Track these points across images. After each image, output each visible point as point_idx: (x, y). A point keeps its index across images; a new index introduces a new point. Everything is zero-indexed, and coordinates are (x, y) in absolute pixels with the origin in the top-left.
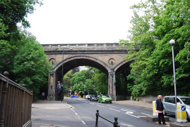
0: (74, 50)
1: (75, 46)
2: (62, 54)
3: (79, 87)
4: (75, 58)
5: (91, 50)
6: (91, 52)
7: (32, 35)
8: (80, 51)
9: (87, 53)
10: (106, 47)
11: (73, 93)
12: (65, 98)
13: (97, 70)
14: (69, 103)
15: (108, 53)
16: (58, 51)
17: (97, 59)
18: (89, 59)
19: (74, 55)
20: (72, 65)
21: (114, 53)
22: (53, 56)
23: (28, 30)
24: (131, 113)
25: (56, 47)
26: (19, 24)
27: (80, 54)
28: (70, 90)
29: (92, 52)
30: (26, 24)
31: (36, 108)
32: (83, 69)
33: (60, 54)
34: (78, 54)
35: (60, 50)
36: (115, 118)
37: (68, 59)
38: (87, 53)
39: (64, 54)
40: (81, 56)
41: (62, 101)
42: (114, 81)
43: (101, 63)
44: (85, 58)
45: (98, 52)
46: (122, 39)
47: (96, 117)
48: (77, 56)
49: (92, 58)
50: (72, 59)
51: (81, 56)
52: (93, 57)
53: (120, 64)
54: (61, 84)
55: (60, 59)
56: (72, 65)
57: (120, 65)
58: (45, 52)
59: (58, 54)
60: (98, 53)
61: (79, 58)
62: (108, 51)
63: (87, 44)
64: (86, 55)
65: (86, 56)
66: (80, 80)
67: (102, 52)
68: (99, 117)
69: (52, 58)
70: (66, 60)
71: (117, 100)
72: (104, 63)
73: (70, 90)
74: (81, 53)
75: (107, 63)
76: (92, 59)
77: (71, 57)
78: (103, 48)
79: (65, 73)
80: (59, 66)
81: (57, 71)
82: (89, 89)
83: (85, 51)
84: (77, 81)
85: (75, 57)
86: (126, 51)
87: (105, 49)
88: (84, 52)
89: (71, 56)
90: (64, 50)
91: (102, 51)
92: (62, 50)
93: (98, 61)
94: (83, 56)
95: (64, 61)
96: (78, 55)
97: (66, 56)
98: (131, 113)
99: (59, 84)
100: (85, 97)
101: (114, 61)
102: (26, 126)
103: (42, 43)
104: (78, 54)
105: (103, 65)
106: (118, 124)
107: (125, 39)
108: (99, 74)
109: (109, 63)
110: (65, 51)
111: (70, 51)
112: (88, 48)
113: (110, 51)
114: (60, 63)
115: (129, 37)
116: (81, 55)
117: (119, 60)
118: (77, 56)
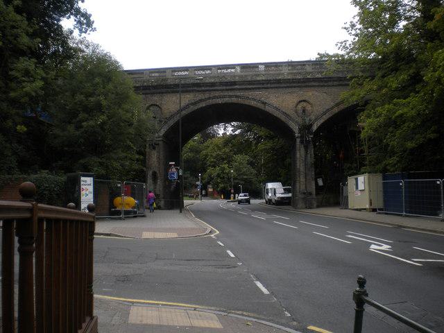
0: (207, 81)
1: (208, 72)
2: (177, 92)
3: (218, 176)
4: (211, 102)
5: (249, 79)
6: (250, 87)
7: (101, 49)
8: (221, 84)
9: (239, 89)
10: (287, 71)
11: (204, 187)
12: (187, 202)
13: (263, 132)
14: (200, 214)
15: (295, 87)
16: (168, 86)
17: (264, 103)
18: (247, 102)
19: (207, 95)
20: (200, 120)
21: (309, 86)
22: (156, 99)
23: (91, 37)
24: (385, 247)
25: (162, 74)
26: (67, 23)
27: (222, 90)
28: (197, 183)
29: (254, 84)
30: (86, 22)
31: (116, 236)
32: (224, 130)
33: (173, 92)
34: (218, 90)
35: (172, 83)
36: (360, 278)
37: (192, 104)
38: (239, 89)
39: (183, 92)
40: (224, 97)
41: (181, 212)
42: (311, 160)
43: (277, 114)
44: (234, 100)
45: (269, 85)
46: (323, 52)
47: (354, 306)
48: (214, 97)
49: (254, 100)
50: (203, 105)
51: (224, 97)
52: (254, 98)
53: (324, 113)
54: (177, 169)
55: (173, 104)
56: (200, 120)
57: (325, 118)
58: (137, 89)
59: (166, 93)
60: (267, 88)
61: (220, 101)
62: (294, 82)
63: (238, 65)
64: (238, 93)
65: (236, 96)
66: (221, 159)
67: (277, 85)
68: (368, 309)
69: (152, 103)
70: (187, 106)
71: (318, 207)
72: (285, 113)
73: (198, 183)
74: (224, 88)
75: (291, 113)
76: (253, 103)
77: (201, 101)
78: (279, 74)
79: (186, 140)
80: (171, 123)
81: (166, 136)
82: (242, 180)
83: (234, 83)
84: (212, 162)
85: (209, 98)
86: (345, 79)
87: (286, 77)
88: (231, 85)
89: (200, 96)
90: (182, 82)
91: (279, 81)
92: (177, 82)
93: (268, 109)
94: (230, 96)
95: (181, 110)
96: (217, 94)
97: (187, 98)
98: (385, 247)
99: (174, 170)
100: (234, 198)
101: (309, 108)
102: (88, 331)
103: (126, 68)
104: (218, 90)
105: (283, 118)
106: (367, 295)
107: (332, 50)
108: (269, 144)
109: (296, 112)
110: (184, 86)
111: (198, 85)
112: (241, 76)
113: (299, 81)
114: (172, 116)
115: (343, 44)
116: (226, 94)
117: (321, 104)
118: (214, 97)
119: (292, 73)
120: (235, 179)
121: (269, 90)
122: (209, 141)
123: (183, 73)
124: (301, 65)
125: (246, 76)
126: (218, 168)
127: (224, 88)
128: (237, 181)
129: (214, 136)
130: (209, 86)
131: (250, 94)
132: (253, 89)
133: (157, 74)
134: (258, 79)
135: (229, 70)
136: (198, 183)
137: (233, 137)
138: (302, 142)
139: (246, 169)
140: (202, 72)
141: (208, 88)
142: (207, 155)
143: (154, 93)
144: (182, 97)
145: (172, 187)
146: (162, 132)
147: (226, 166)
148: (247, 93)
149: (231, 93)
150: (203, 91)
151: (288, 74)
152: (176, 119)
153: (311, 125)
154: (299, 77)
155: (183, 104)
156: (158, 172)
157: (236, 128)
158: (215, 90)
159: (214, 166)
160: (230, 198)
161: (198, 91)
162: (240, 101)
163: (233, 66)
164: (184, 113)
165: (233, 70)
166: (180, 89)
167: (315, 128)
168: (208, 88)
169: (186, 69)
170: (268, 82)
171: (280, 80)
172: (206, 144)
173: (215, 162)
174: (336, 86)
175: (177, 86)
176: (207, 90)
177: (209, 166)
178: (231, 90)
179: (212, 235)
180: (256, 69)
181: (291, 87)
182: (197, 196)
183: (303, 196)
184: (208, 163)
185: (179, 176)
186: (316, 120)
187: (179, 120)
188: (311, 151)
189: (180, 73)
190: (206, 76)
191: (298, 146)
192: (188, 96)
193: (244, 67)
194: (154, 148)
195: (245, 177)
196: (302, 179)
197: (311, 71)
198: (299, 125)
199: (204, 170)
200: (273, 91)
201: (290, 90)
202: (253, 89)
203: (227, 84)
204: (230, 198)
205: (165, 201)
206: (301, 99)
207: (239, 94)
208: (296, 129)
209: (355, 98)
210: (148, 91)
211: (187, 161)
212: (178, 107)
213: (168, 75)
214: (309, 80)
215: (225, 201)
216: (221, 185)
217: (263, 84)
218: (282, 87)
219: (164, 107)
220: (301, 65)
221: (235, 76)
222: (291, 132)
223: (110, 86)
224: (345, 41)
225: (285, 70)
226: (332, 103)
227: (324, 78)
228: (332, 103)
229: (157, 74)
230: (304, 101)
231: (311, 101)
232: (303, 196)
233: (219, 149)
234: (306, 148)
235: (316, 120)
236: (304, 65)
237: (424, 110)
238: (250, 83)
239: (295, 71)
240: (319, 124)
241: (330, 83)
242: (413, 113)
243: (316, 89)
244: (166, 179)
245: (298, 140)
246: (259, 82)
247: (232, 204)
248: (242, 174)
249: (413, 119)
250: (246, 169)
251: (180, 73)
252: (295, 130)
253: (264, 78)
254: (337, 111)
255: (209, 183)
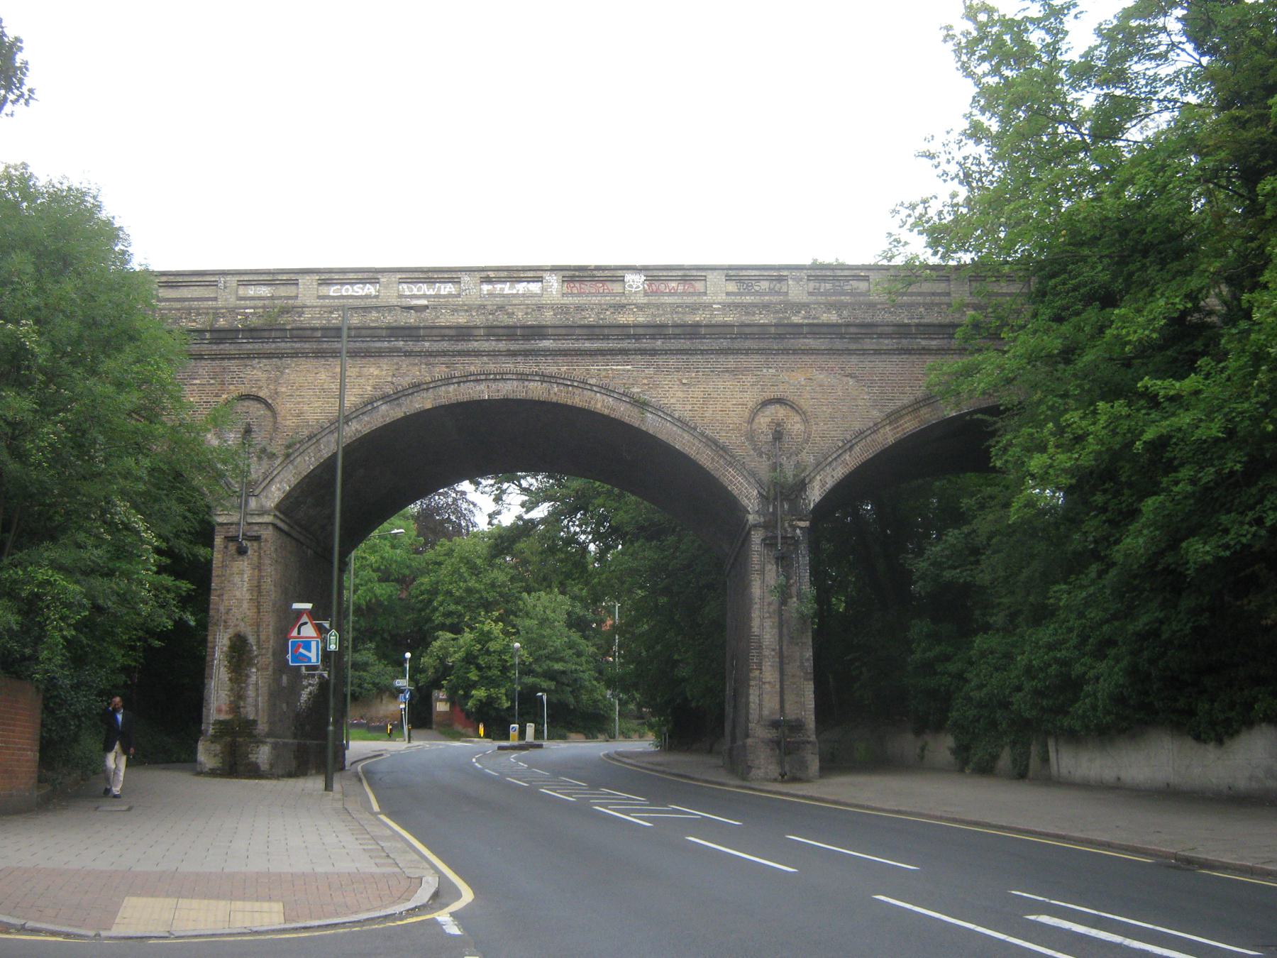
0: (442, 321)
1: (447, 289)
2: (335, 354)
3: (470, 659)
6: (597, 345)
8: (493, 331)
10: (722, 298)
12: (358, 747)
15: (748, 352)
16: (302, 334)
17: (642, 405)
18: (578, 399)
21: (795, 352)
22: (256, 376)
25: (283, 291)
27: (493, 354)
29: (606, 338)
33: (319, 354)
34: (478, 353)
35: (316, 323)
37: (386, 398)
39: (354, 354)
40: (501, 377)
41: (328, 787)
44: (536, 390)
48: (466, 379)
49: (607, 391)
50: (425, 402)
51: (501, 377)
53: (848, 446)
57: (851, 461)
59: (295, 355)
60: (654, 352)
61: (483, 391)
62: (745, 336)
63: (554, 269)
65: (544, 378)
67: (686, 344)
69: (244, 390)
70: (369, 405)
72: (712, 443)
74: (502, 346)
76: (601, 403)
77: (417, 387)
78: (694, 308)
80: (307, 463)
81: (287, 507)
82: (550, 675)
83: (537, 332)
85: (447, 381)
87: (719, 318)
88: (526, 338)
89: (415, 372)
90: (355, 320)
91: (692, 331)
92: (335, 319)
93: (651, 424)
94: (523, 377)
96: (475, 365)
99: (309, 631)
101: (795, 425)
104: (478, 353)
105: (704, 457)
110: (361, 332)
112: (563, 309)
113: (761, 332)
118: (466, 379)
119: (737, 306)
120: (527, 671)
121: (660, 360)
122: (444, 544)
123: (358, 290)
124: (770, 279)
125: (579, 308)
126: (468, 636)
127: (502, 346)
128: (529, 680)
129: (458, 530)
130: (451, 338)
131: (595, 370)
132: (602, 352)
133: (264, 291)
134: (623, 319)
135: (521, 288)
136: (402, 683)
137: (523, 529)
138: (769, 543)
139: (560, 636)
140: (425, 289)
141: (445, 345)
142: (434, 592)
143: (249, 356)
144: (352, 372)
145: (304, 696)
146: (275, 493)
147: (497, 628)
148: (580, 369)
149: (523, 366)
150: (431, 354)
151: (726, 306)
152: (328, 447)
153: (802, 486)
154: (762, 319)
155: (351, 399)
156: (252, 640)
157: (534, 499)
158: (467, 353)
159: (456, 629)
160: (507, 738)
161: (408, 354)
162: (556, 394)
163: (534, 274)
164: (355, 429)
165: (535, 287)
166: (344, 345)
167: (815, 494)
168: (445, 345)
169: (370, 275)
170: (657, 331)
171: (697, 325)
172: (430, 554)
173: (461, 616)
174: (888, 352)
175: (334, 332)
176: (444, 353)
177: (442, 627)
178: (526, 353)
179: (443, 917)
180: (617, 288)
181: (736, 352)
182: (398, 727)
183: (770, 734)
184: (438, 618)
185: (326, 655)
186: (819, 466)
187: (335, 455)
188: (804, 582)
189: (347, 290)
190: (438, 304)
191: (755, 558)
192: (374, 371)
193: (575, 275)
194: (242, 551)
195: (558, 666)
196: (769, 673)
197: (805, 299)
198: (760, 483)
199: (420, 641)
200: (672, 361)
201: (731, 362)
202: (602, 352)
203: (511, 332)
204: (507, 738)
205: (275, 747)
206: (768, 395)
207: (552, 369)
208: (748, 496)
209: (980, 383)
210: (227, 348)
211: (369, 610)
212: (332, 408)
213: (307, 293)
214: (797, 330)
215: (491, 745)
216: (480, 693)
217: (637, 337)
218: (703, 352)
219: (285, 407)
220: (770, 279)
221: (540, 308)
222: (731, 505)
223: (69, 287)
224: (924, 202)
225: (718, 292)
226: (875, 413)
227: (848, 325)
228: (875, 413)
229: (264, 291)
230: (780, 401)
231: (805, 403)
232: (770, 734)
233: (475, 570)
234: (783, 560)
235: (819, 466)
236: (781, 279)
237: (1256, 420)
238: (593, 331)
239: (749, 299)
240: (830, 483)
241: (869, 344)
242: (1214, 429)
243: (821, 360)
244: (281, 666)
245: (757, 537)
246: (624, 331)
247: (513, 756)
248: (548, 657)
249: (1206, 451)
250: (560, 636)
251: (347, 290)
252: (745, 502)
253: (641, 319)
254: (891, 440)
255: (436, 684)
